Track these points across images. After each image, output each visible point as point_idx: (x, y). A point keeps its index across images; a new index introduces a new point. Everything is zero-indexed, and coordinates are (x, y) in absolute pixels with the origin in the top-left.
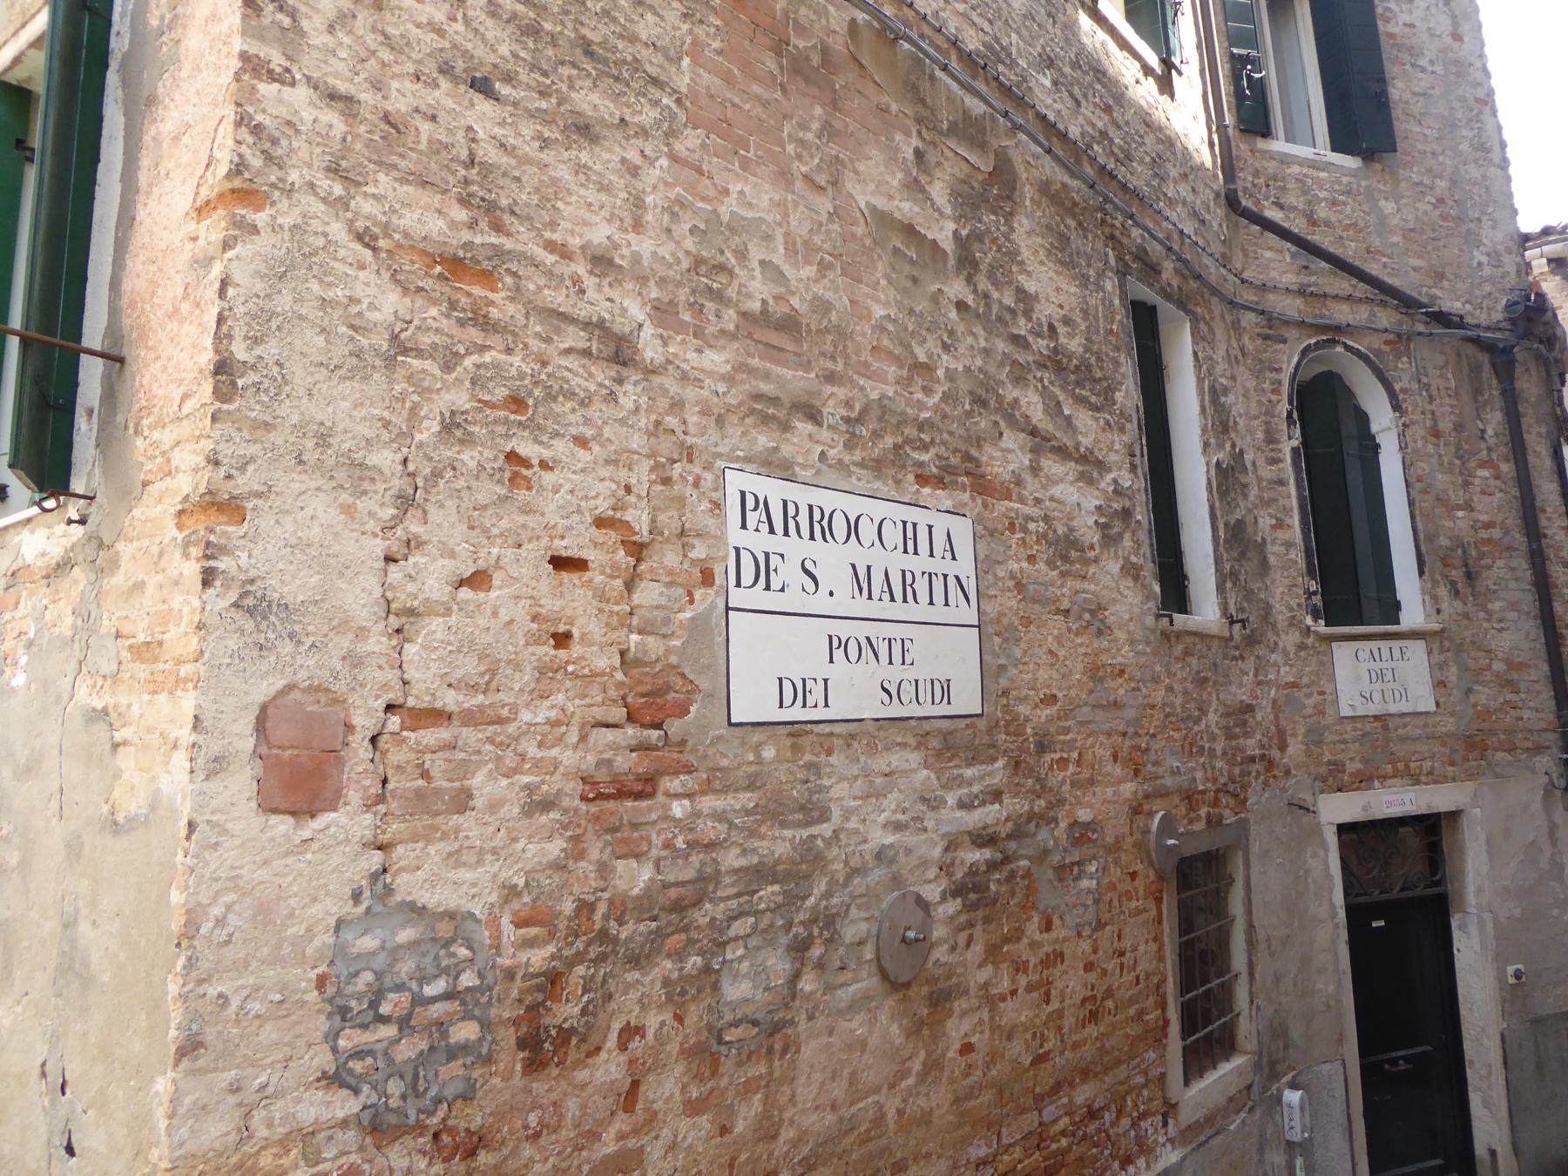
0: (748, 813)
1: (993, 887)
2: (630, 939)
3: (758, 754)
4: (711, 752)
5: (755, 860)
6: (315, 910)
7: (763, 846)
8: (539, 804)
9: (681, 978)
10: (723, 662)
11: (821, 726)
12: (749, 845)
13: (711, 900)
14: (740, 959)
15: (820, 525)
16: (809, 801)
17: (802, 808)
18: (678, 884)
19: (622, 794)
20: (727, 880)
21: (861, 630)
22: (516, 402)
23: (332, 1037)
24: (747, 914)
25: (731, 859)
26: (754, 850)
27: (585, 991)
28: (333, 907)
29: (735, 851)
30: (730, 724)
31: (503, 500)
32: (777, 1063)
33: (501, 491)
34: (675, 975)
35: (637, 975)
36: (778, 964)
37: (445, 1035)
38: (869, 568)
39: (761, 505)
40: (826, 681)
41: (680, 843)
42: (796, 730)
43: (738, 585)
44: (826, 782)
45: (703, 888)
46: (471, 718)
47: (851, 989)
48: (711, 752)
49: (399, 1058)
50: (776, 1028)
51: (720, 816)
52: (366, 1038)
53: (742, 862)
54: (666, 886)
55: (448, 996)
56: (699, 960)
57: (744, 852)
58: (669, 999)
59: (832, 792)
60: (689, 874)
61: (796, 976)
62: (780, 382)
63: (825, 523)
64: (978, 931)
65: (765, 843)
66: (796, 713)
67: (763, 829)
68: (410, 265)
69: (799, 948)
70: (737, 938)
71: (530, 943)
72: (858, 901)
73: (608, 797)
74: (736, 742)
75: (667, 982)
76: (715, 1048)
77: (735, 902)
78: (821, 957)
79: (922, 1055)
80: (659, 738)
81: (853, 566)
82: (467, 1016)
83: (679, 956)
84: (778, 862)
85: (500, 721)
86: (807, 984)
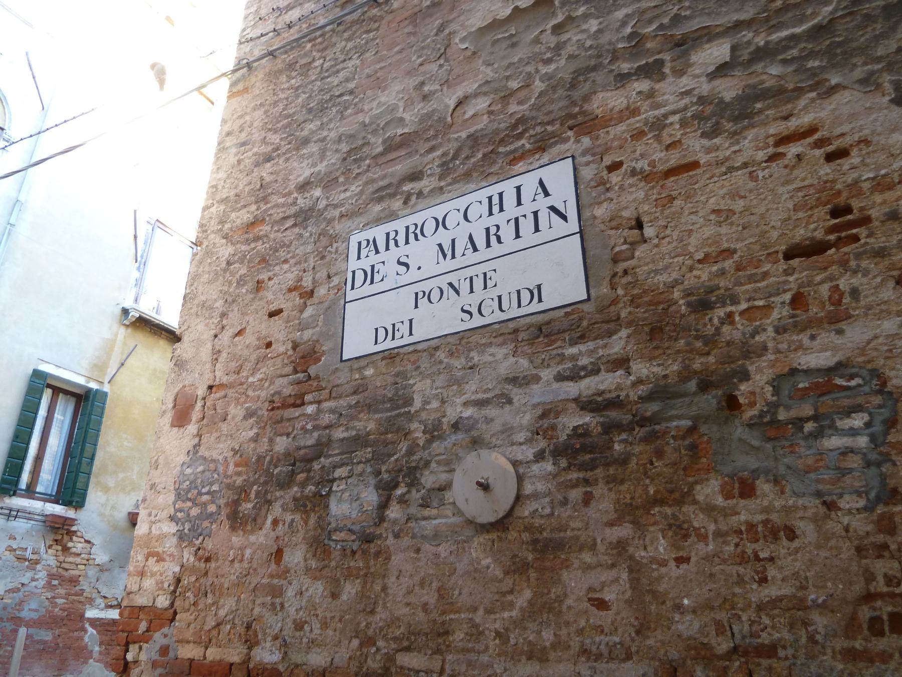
0: (350, 407)
1: (617, 447)
2: (279, 474)
3: (361, 374)
4: (332, 378)
5: (354, 433)
6: (178, 459)
7: (359, 425)
8: (249, 414)
9: (302, 496)
10: (340, 331)
11: (406, 348)
12: (351, 424)
13: (325, 457)
14: (343, 491)
15: (419, 232)
16: (396, 394)
17: (391, 400)
18: (305, 447)
19: (285, 406)
20: (336, 445)
21: (443, 282)
22: (263, 260)
23: (174, 504)
24: (347, 464)
25: (339, 434)
26: (353, 428)
27: (256, 497)
28: (183, 458)
29: (341, 429)
30: (342, 361)
31: (253, 299)
32: (372, 562)
33: (252, 296)
34: (299, 495)
35: (282, 493)
36: (371, 497)
37: (206, 507)
38: (453, 241)
39: (371, 242)
40: (411, 321)
41: (309, 427)
42: (390, 356)
43: (353, 288)
44: (411, 382)
45: (320, 449)
46: (230, 386)
47: (434, 522)
48: (332, 378)
49: (191, 515)
50: (368, 539)
51: (332, 411)
52: (184, 505)
53: (346, 435)
54: (299, 448)
55: (208, 493)
56: (313, 488)
57: (347, 429)
58: (476, 570)
59: (415, 388)
60: (311, 442)
61: (383, 506)
62: (392, 175)
63: (418, 231)
64: (599, 490)
65: (362, 423)
66: (389, 344)
67: (362, 415)
68: (856, 86)
69: (386, 489)
70: (340, 479)
71: (238, 474)
72: (437, 458)
73: (278, 408)
74: (346, 370)
75: (295, 499)
76: (326, 541)
77: (339, 457)
78: (403, 495)
79: (528, 594)
80: (304, 377)
81: (440, 246)
82: (213, 502)
83: (303, 485)
84: (368, 434)
85: (242, 384)
86: (394, 512)
